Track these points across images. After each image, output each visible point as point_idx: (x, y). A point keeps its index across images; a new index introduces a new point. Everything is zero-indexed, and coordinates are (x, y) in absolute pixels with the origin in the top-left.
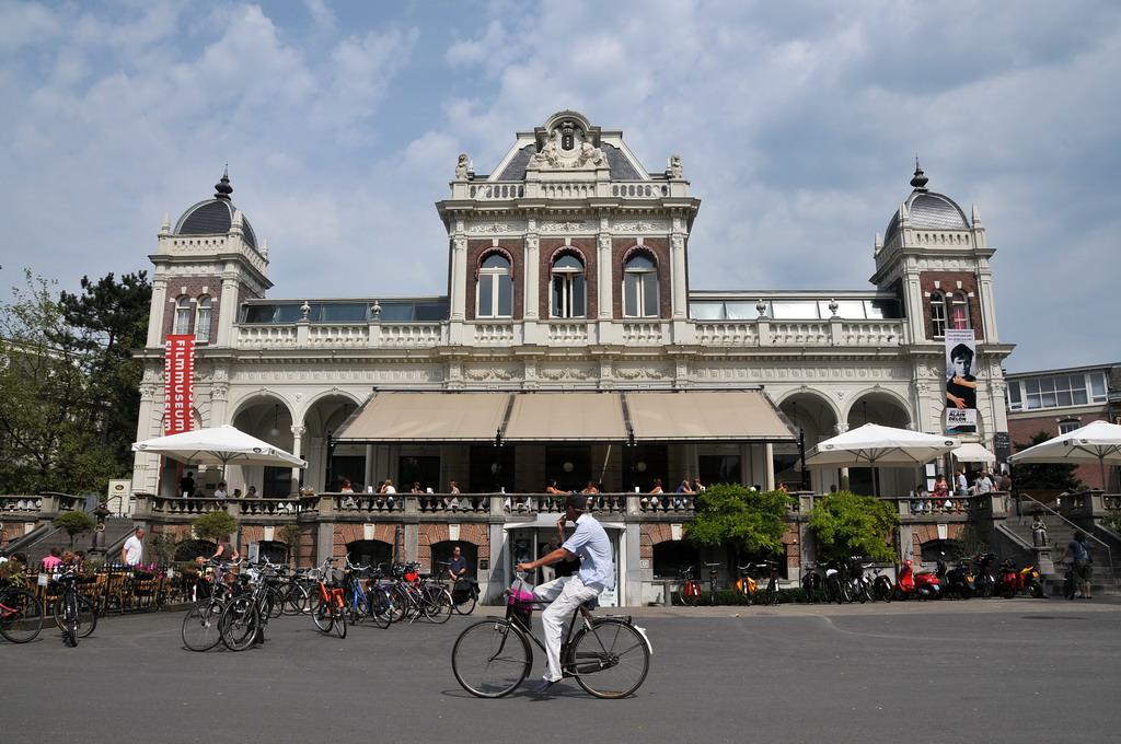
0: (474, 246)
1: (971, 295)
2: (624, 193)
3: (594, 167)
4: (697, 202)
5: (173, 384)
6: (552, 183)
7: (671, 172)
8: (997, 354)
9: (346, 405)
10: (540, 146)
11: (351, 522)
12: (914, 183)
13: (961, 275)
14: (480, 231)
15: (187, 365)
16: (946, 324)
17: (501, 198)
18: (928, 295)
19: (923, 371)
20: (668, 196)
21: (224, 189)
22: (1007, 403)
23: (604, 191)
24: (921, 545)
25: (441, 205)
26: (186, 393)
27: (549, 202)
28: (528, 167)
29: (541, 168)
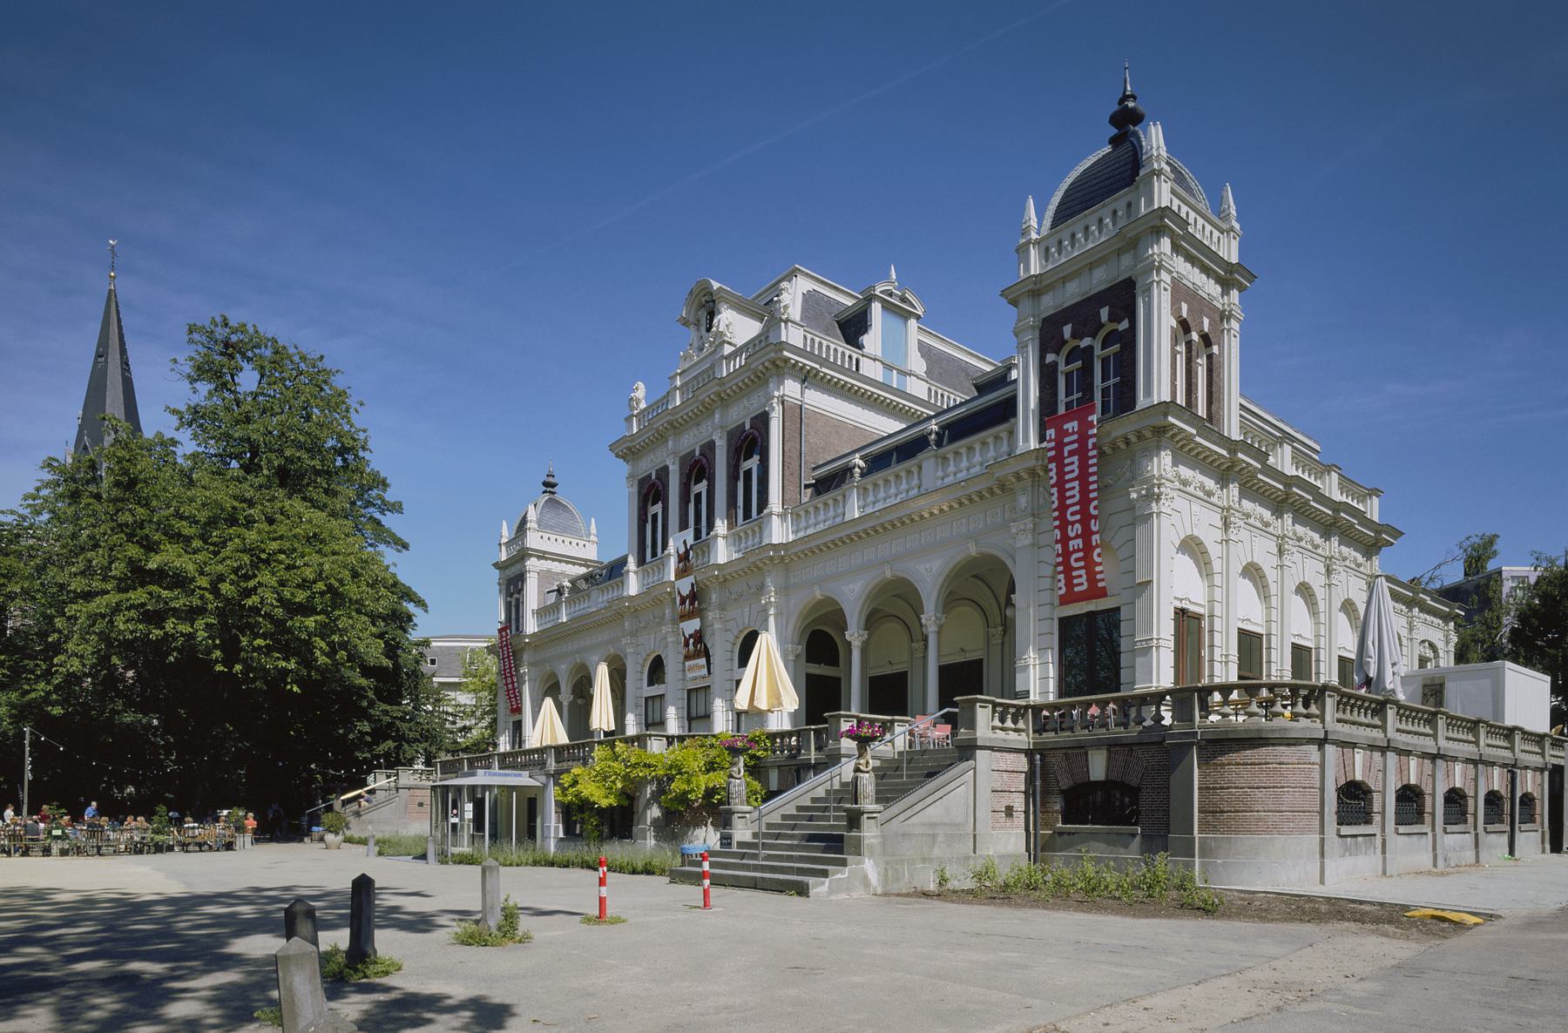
5: (1063, 508)
15: (1084, 466)
26: (1086, 519)
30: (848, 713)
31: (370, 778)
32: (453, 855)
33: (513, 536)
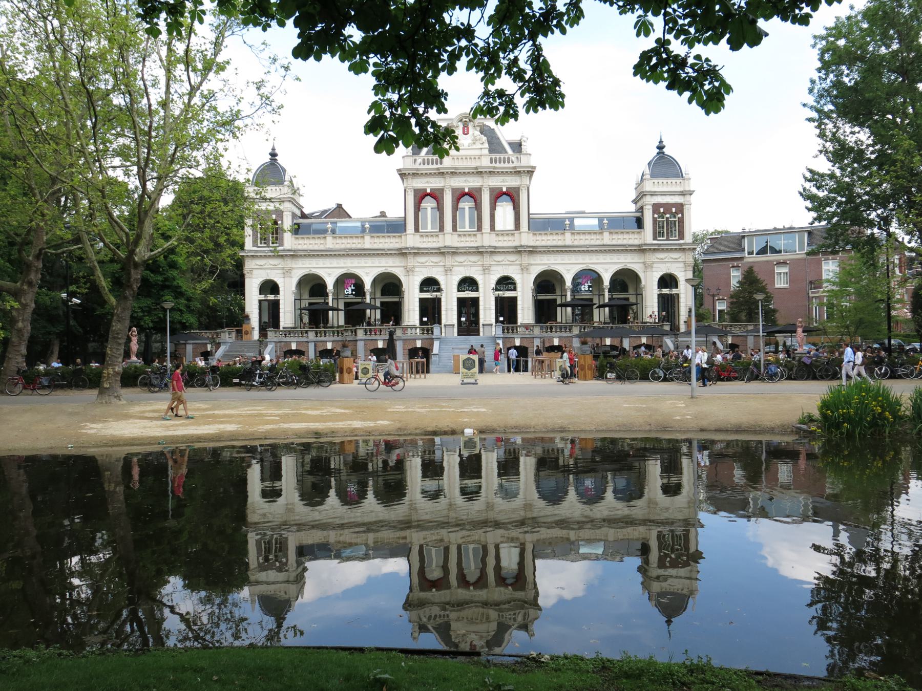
0: (416, 191)
4: (534, 168)
12: (658, 148)
19: (487, 260)
21: (273, 155)
25: (399, 170)
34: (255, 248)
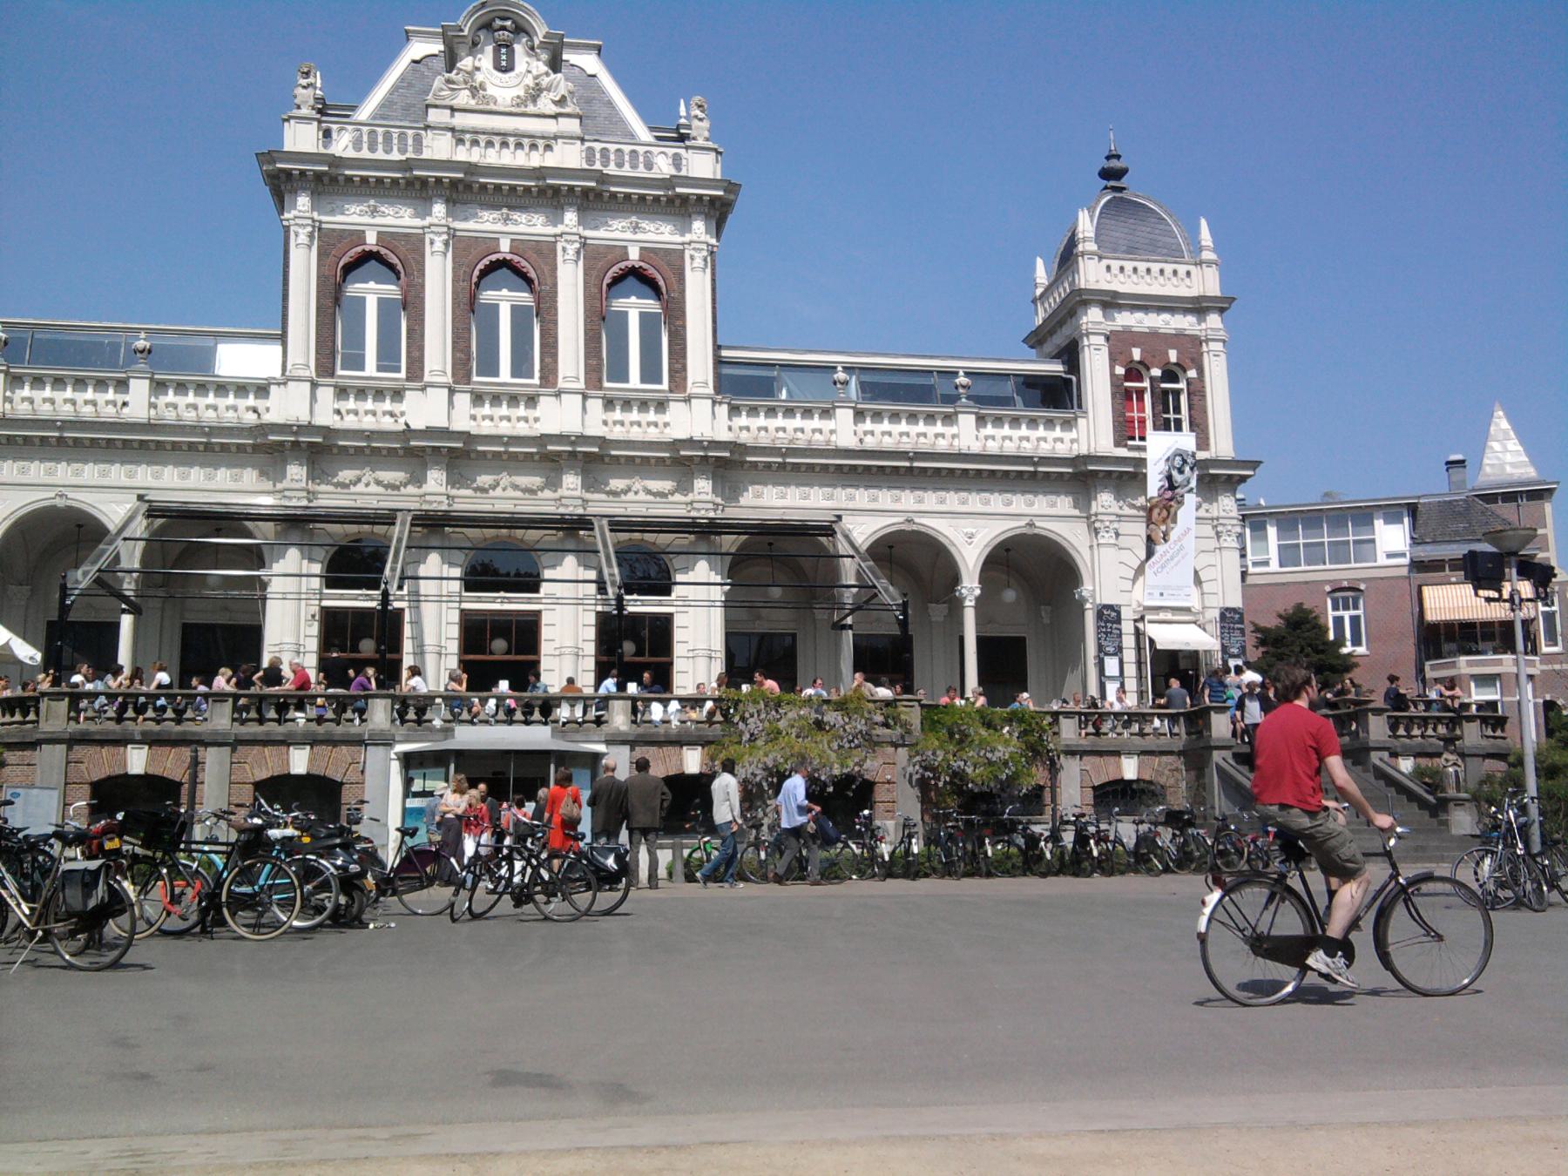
1: (1192, 373)
2: (606, 163)
3: (554, 109)
6: (476, 133)
7: (689, 127)
8: (1230, 476)
9: (79, 526)
10: (451, 61)
11: (102, 743)
13: (1178, 339)
14: (485, 222)
16: (1149, 424)
17: (380, 155)
18: (1120, 371)
19: (1105, 501)
20: (410, 155)
22: (1243, 556)
23: (568, 156)
24: (1094, 788)
27: (470, 168)
28: (430, 99)
29: (454, 103)
30: (185, 789)
31: (464, 806)
32: (1192, 706)
33: (1052, 279)
34: (1122, 452)
